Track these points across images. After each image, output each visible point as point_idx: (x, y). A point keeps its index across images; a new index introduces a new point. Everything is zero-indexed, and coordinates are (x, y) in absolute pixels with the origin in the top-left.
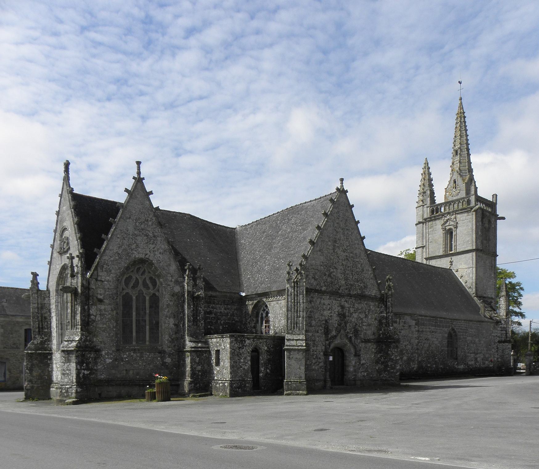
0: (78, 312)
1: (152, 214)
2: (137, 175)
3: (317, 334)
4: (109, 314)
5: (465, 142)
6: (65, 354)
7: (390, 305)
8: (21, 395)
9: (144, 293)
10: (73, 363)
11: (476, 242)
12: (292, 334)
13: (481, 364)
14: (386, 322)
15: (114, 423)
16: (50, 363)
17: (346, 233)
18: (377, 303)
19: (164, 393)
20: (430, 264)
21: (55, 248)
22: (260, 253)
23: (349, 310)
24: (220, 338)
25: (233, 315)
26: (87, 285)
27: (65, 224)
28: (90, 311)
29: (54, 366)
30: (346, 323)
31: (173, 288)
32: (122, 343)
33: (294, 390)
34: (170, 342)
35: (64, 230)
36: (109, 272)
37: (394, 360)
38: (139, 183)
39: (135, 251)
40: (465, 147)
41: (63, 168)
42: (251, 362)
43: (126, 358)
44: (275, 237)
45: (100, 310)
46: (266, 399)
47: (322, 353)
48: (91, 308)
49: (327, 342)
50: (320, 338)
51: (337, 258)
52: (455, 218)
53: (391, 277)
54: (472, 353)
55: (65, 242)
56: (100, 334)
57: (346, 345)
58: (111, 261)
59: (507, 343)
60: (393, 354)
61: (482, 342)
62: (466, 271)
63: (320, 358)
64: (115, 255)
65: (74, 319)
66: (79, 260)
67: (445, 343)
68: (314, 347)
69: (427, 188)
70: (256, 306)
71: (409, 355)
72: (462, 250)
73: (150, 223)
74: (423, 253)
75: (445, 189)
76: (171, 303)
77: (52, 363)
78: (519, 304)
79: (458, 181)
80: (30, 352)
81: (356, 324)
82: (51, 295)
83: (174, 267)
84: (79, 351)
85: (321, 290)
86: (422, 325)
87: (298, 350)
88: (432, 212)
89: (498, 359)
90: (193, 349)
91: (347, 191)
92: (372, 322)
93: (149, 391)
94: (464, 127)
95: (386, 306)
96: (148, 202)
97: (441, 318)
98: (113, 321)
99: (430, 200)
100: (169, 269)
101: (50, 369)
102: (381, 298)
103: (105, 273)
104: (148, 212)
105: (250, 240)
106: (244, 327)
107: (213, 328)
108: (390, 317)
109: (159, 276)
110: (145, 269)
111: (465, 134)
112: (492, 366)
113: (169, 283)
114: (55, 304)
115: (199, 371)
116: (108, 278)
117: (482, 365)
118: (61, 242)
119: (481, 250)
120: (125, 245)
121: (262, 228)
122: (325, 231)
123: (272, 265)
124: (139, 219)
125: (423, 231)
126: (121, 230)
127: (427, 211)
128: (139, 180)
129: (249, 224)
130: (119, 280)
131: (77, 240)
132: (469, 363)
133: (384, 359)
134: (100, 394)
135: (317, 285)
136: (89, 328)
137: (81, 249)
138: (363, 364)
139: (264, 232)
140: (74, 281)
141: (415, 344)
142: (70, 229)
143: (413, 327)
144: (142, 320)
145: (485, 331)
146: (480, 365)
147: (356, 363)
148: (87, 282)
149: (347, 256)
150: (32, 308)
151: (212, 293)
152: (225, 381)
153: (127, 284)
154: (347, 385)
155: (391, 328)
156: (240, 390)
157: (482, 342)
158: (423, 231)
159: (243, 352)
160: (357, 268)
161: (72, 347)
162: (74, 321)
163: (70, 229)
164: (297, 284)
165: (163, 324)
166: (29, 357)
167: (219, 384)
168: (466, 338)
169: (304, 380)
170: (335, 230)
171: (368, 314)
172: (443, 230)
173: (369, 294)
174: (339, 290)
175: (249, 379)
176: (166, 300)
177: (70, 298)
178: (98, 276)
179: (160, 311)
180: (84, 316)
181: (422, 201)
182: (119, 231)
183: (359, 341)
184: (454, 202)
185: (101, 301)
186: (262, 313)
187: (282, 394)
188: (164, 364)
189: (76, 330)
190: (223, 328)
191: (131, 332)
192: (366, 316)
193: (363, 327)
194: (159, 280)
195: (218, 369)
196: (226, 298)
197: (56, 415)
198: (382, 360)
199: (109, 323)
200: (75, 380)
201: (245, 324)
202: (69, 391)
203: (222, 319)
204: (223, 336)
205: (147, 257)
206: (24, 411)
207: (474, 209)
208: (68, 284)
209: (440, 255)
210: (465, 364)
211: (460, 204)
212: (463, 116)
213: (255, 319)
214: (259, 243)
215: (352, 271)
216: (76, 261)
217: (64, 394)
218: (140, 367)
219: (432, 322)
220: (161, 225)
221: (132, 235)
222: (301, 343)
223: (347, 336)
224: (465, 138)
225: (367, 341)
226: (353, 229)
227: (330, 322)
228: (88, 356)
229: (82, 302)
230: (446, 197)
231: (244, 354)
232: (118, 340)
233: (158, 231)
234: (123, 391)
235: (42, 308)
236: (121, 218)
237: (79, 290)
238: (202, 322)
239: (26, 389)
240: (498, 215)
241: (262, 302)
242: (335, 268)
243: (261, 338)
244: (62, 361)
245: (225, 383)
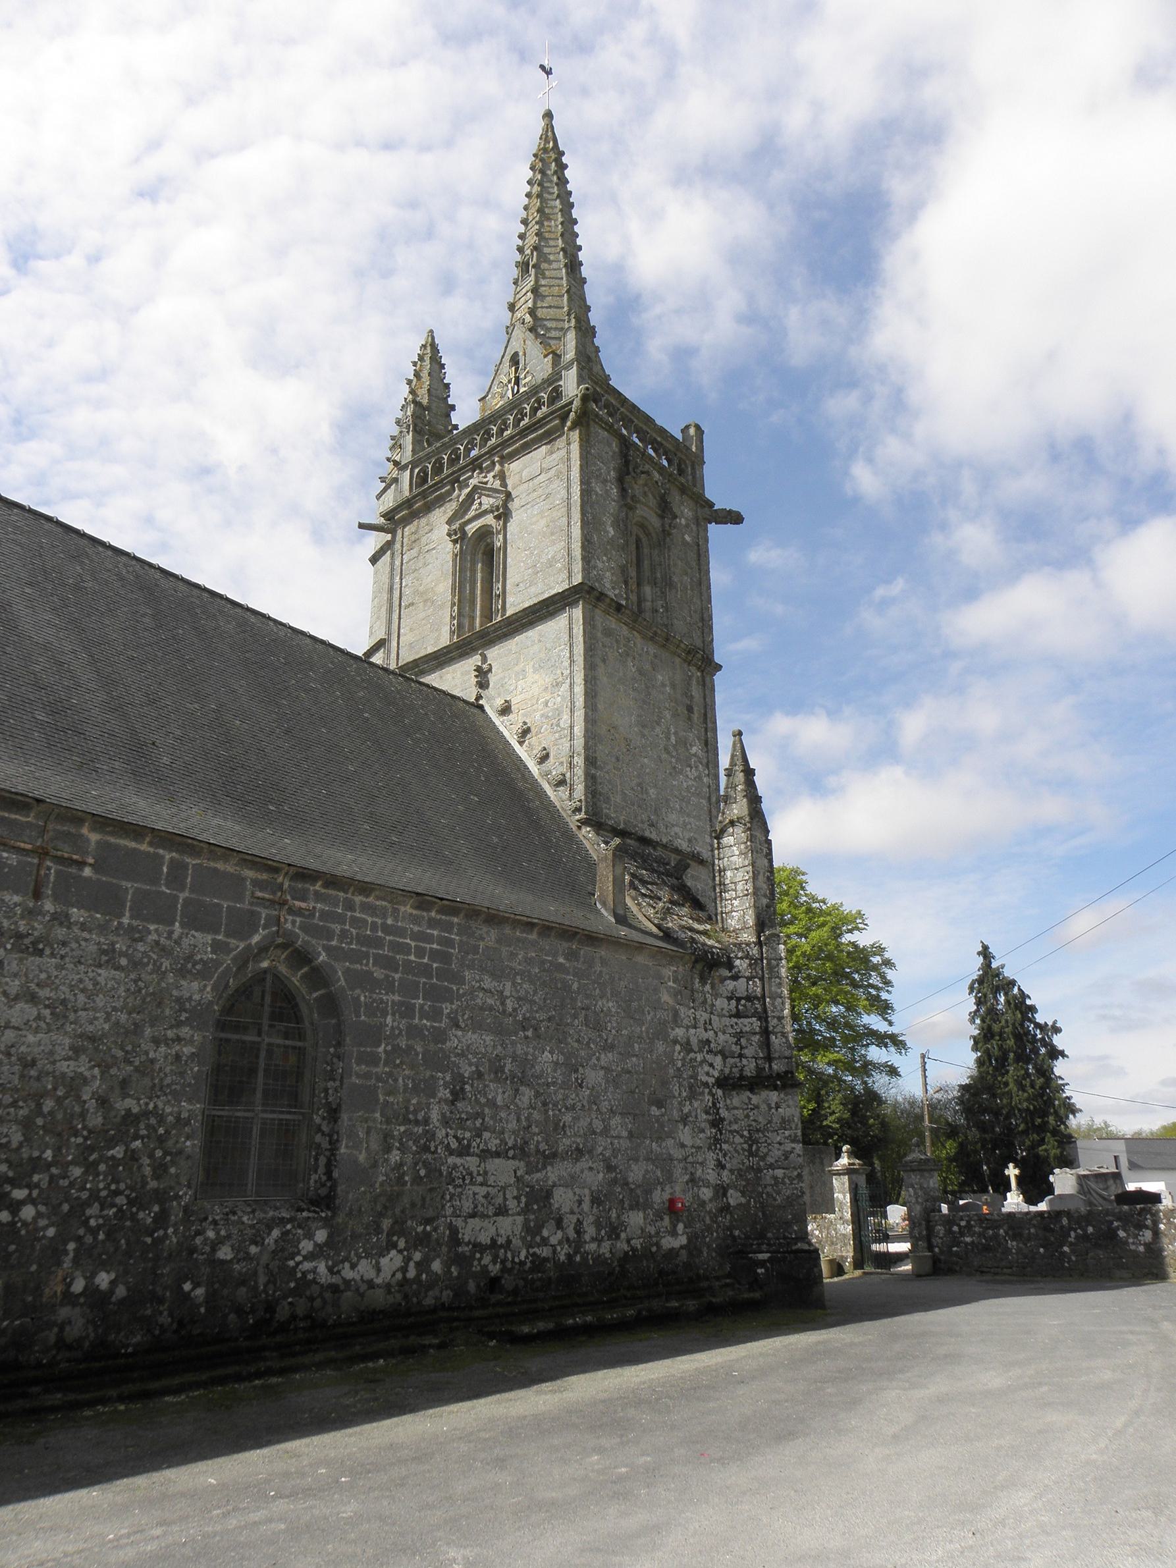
13: (590, 1231)
52: (502, 476)
59: (775, 1088)
61: (594, 1077)
78: (884, 1009)
79: (525, 354)
112: (683, 1240)
117: (598, 1240)
146: (577, 1243)
168: (440, 1036)
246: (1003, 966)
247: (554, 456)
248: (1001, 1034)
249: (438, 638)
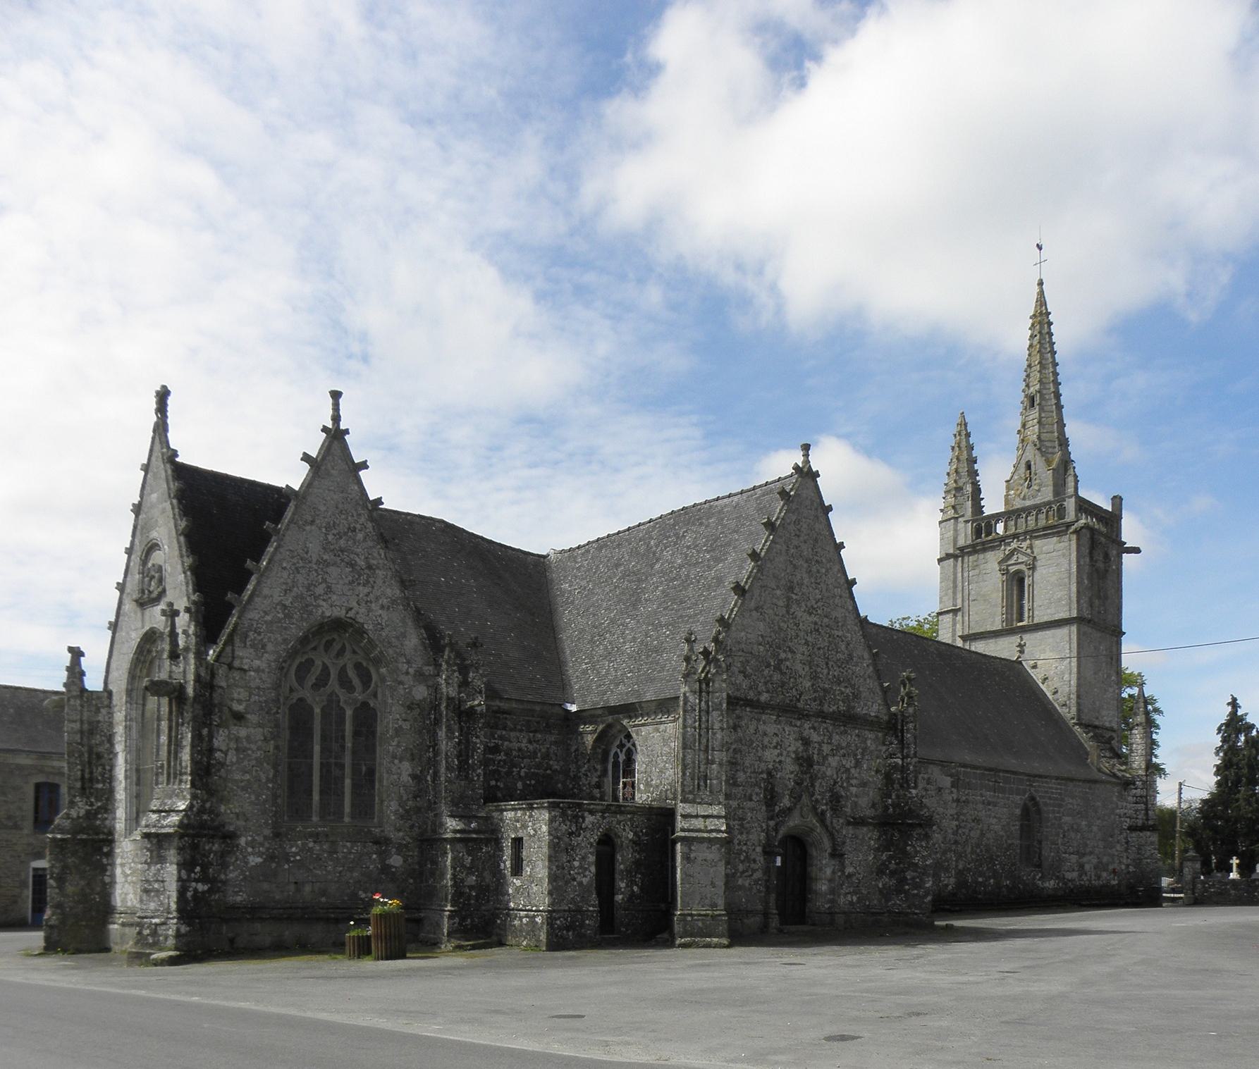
0: (184, 743)
1: (365, 513)
2: (331, 422)
3: (749, 803)
4: (258, 749)
5: (1052, 379)
6: (151, 842)
7: (912, 740)
8: (36, 938)
9: (342, 700)
11: (1078, 602)
12: (693, 802)
13: (1093, 877)
14: (903, 778)
15: (303, 1014)
16: (108, 864)
17: (814, 569)
18: (880, 734)
20: (973, 649)
21: (128, 590)
22: (610, 613)
23: (819, 750)
24: (523, 809)
25: (547, 756)
26: (208, 678)
27: (154, 534)
28: (214, 740)
29: (118, 871)
30: (813, 779)
31: (411, 690)
32: (286, 818)
33: (699, 935)
34: (402, 817)
35: (152, 547)
36: (260, 648)
37: (920, 868)
38: (336, 442)
39: (324, 600)
40: (1052, 390)
41: (152, 404)
42: (596, 867)
43: (296, 854)
44: (647, 578)
45: (237, 739)
46: (637, 957)
47: (759, 849)
48: (216, 735)
49: (772, 823)
50: (756, 813)
51: (795, 627)
52: (1031, 547)
53: (913, 675)
54: (1072, 854)
55: (153, 577)
56: (236, 795)
57: (812, 830)
58: (266, 622)
59: (1149, 830)
60: (917, 852)
61: (1095, 829)
62: (1056, 668)
63: (755, 861)
64: (275, 608)
65: (176, 758)
66: (190, 620)
67: (1015, 830)
68: (741, 833)
69: (965, 479)
70: (602, 738)
71: (938, 856)
72: (1046, 619)
73: (360, 536)
74: (954, 624)
75: (1007, 481)
76: (406, 726)
77: (113, 865)
79: (1035, 464)
80: (59, 836)
81: (835, 783)
82: (114, 702)
83: (413, 641)
84: (187, 835)
85: (758, 700)
86: (965, 788)
87: (710, 840)
88: (978, 532)
89: (1128, 866)
90: (458, 835)
91: (817, 474)
92: (870, 776)
93: (353, 933)
94: (1048, 345)
95: (902, 742)
96: (356, 488)
97: (1007, 772)
98: (268, 764)
99: (973, 505)
100: (402, 644)
101: (107, 879)
102: (889, 722)
103: (252, 650)
104: (356, 510)
105: (583, 583)
106: (574, 785)
107: (502, 786)
108: (911, 767)
109: (377, 662)
110: (344, 644)
111: (1050, 360)
112: (1117, 882)
113: (402, 678)
114: (124, 724)
115: (471, 888)
116: (257, 663)
117: (1095, 880)
118: (143, 578)
119: (1089, 621)
120: (299, 585)
121: (613, 557)
122: (769, 565)
123: (642, 641)
124: (334, 526)
125: (955, 574)
126: (291, 551)
127: (966, 529)
128: (336, 436)
129: (579, 547)
130: (283, 668)
131: (184, 573)
132: (1066, 877)
133: (896, 864)
134: (232, 941)
135: (751, 688)
136: (209, 781)
137: (194, 594)
138: (850, 876)
139: (617, 566)
140: (178, 670)
141: (950, 831)
142: (166, 547)
143: (947, 791)
144: (336, 764)
145: (1099, 804)
147: (834, 872)
148: (209, 672)
149: (816, 623)
150: (70, 728)
151: (502, 704)
152: (535, 911)
153: (301, 679)
154: (814, 925)
155: (914, 792)
156: (570, 933)
157: (1095, 829)
158: (955, 574)
159: (578, 844)
160: (837, 652)
161: (170, 826)
162: (175, 765)
163: (166, 547)
164: (708, 685)
165: (385, 775)
166: (57, 850)
167: (521, 918)
169: (724, 913)
170: (791, 562)
171: (862, 759)
172: (1003, 574)
173: (864, 712)
174: (799, 701)
175: (591, 909)
176: (392, 717)
177: (167, 709)
178: (233, 658)
179: (377, 743)
180: (199, 752)
181: (954, 507)
182: (288, 553)
183: (841, 821)
184: (1027, 511)
185: (239, 717)
187: (669, 943)
188: (386, 869)
190: (525, 785)
191: (309, 792)
192: (858, 764)
193: (851, 788)
194: (378, 671)
195: (518, 882)
196: (533, 716)
197: (142, 993)
198: (893, 866)
199: (257, 771)
200: (173, 906)
201: (576, 778)
202: (160, 932)
203: (523, 765)
204: (532, 804)
205: (351, 614)
206: (54, 981)
207: (1073, 528)
208: (163, 675)
209: (994, 629)
210: (1058, 877)
211: (1042, 516)
212: (1046, 320)
213: (599, 767)
214: (607, 589)
215: (828, 658)
216: (183, 620)
217: (146, 939)
218: (330, 877)
219: (988, 780)
220: (386, 542)
221: (318, 563)
222: (715, 825)
223: (815, 808)
224: (1051, 370)
225: (858, 822)
226: (830, 561)
227: (778, 776)
228: (207, 848)
229: (194, 719)
230: (1007, 502)
231: (581, 848)
232: (276, 812)
233: (379, 555)
234: (287, 933)
235: (91, 732)
236: (291, 521)
237: (190, 691)
238: (479, 771)
239: (47, 925)
240: (1125, 543)
241: (618, 727)
242: (790, 650)
243: (620, 810)
244: (143, 860)
245: (534, 916)
246: (1246, 714)
247: (1061, 544)
248: (1237, 765)
249: (993, 622)
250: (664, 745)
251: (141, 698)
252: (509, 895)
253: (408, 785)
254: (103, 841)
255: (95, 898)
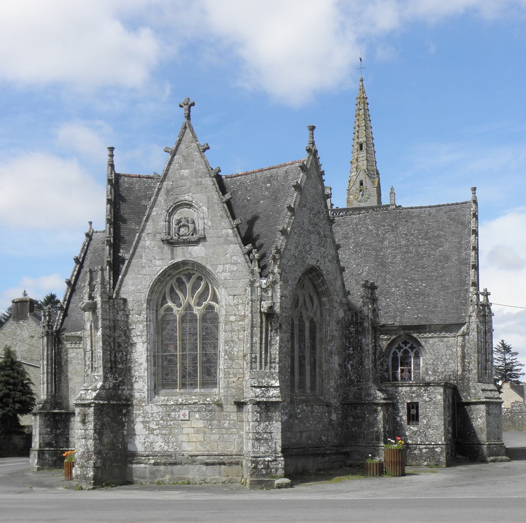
6: (261, 408)
10: (277, 421)
19: (393, 463)
43: (300, 414)
96: (320, 187)
152: (434, 445)
186: (395, 352)
189: (270, 369)
202: (271, 466)
250: (447, 350)
251: (155, 306)
252: (406, 436)
253: (337, 370)
254: (123, 405)
255: (119, 446)
